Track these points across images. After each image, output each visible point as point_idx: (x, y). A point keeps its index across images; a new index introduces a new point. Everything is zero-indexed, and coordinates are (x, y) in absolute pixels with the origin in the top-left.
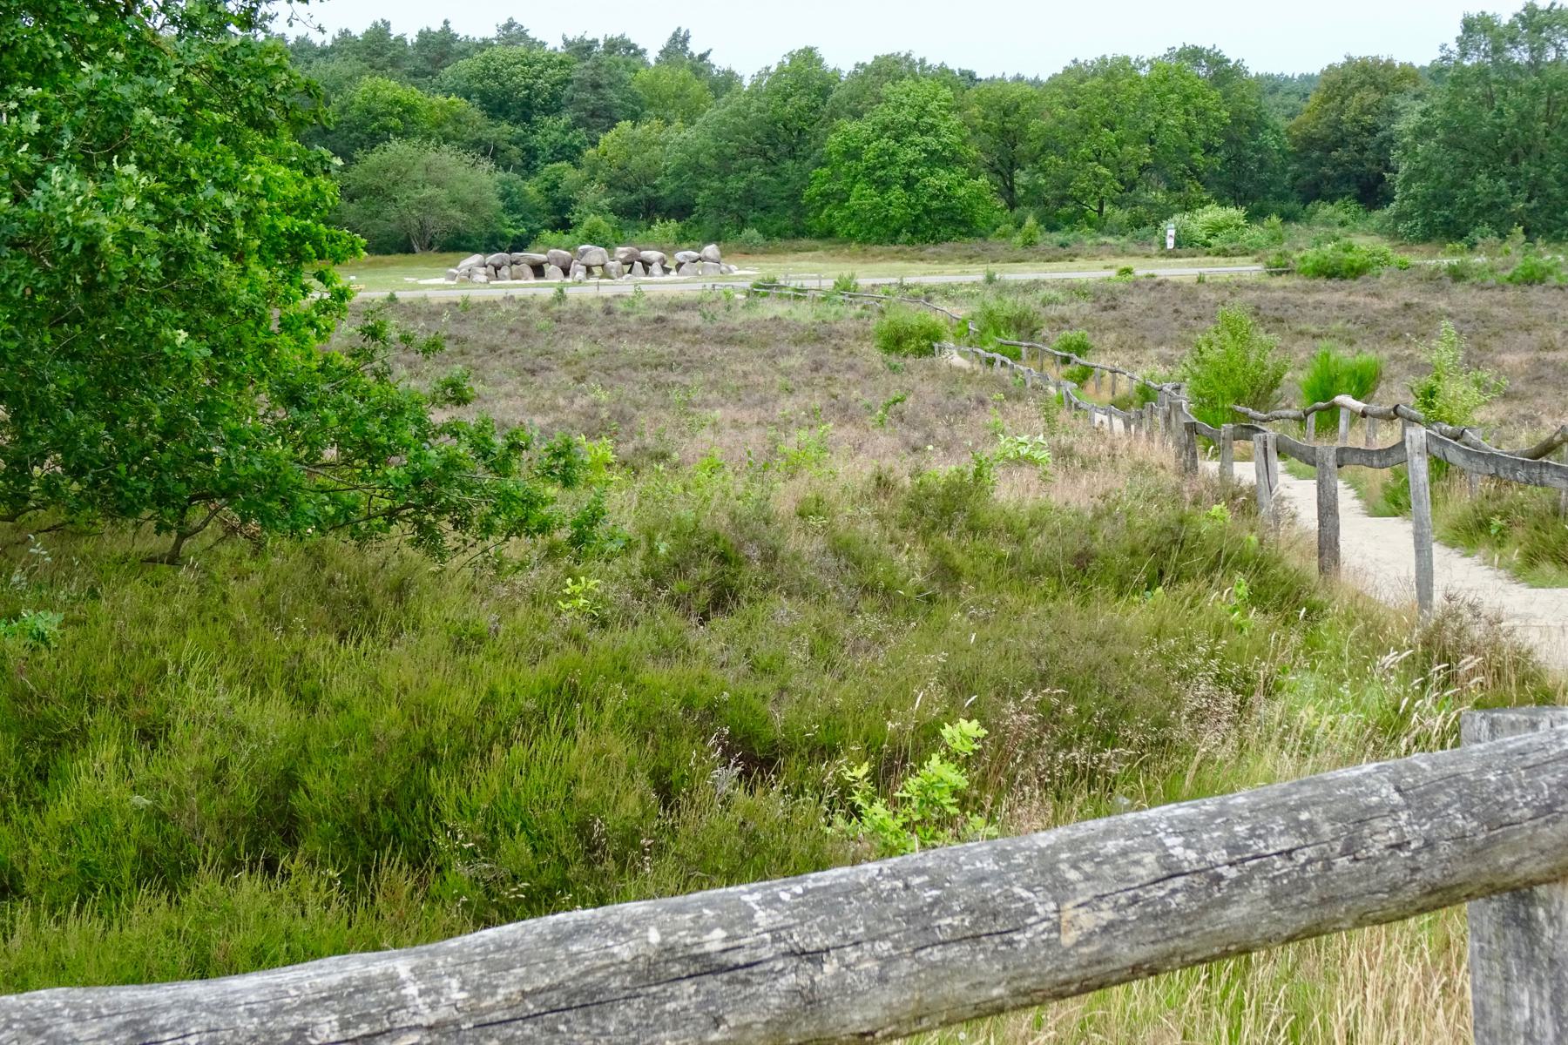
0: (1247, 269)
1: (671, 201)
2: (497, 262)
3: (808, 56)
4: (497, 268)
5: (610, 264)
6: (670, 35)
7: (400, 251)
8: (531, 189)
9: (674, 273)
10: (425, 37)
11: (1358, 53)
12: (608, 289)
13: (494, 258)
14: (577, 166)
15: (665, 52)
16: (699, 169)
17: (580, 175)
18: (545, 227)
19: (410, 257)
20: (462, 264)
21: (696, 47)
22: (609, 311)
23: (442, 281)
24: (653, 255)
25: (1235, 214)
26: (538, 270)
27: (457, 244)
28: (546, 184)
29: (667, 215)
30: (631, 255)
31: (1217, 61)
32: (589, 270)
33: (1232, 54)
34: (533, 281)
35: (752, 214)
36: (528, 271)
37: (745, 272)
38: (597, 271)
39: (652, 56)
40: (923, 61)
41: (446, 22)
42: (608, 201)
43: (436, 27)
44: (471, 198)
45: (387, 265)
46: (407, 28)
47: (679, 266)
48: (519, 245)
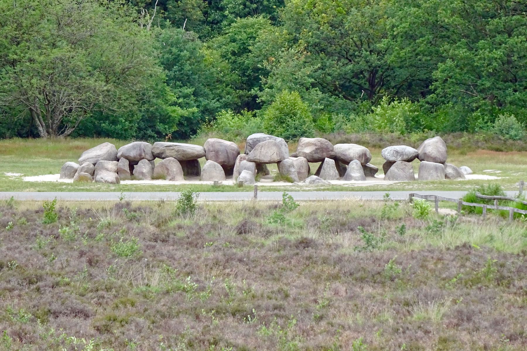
1: (403, 74)
2: (133, 154)
4: (133, 163)
5: (289, 160)
7: (20, 135)
8: (211, 53)
9: (380, 175)
13: (131, 147)
14: (275, 21)
16: (441, 32)
17: (280, 33)
18: (226, 106)
19: (30, 143)
20: (85, 156)
23: (55, 178)
24: (352, 150)
27: (95, 126)
28: (234, 47)
29: (399, 92)
30: (321, 149)
32: (261, 168)
34: (181, 181)
35: (511, 95)
36: (176, 167)
38: (273, 169)
42: (308, 70)
44: (119, 64)
47: (389, 164)
48: (186, 131)
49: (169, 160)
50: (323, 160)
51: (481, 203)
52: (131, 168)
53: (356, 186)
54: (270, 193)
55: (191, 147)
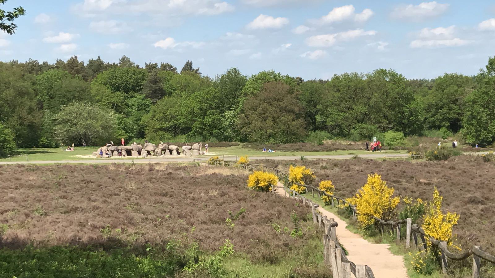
0: (404, 155)
3: (235, 71)
6: (185, 63)
10: (91, 62)
11: (449, 72)
12: (153, 160)
15: (184, 69)
21: (194, 67)
22: (151, 170)
25: (401, 134)
26: (129, 152)
31: (393, 75)
32: (149, 153)
33: (398, 72)
34: (127, 157)
37: (210, 154)
39: (179, 71)
40: (279, 74)
41: (99, 57)
43: (95, 58)
45: (230, 146)
46: (84, 59)
49: (62, 177)
50: (166, 150)
51: (215, 162)
52: (112, 153)
53: (396, 158)
54: (153, 160)
55: (128, 147)
